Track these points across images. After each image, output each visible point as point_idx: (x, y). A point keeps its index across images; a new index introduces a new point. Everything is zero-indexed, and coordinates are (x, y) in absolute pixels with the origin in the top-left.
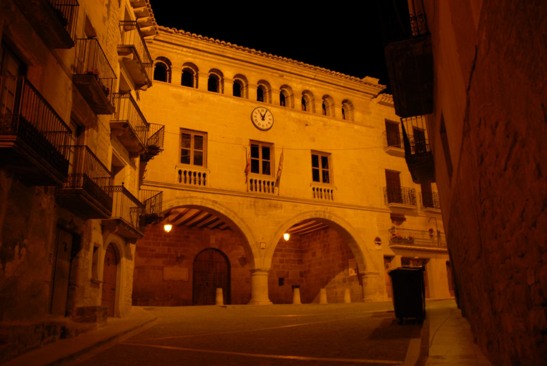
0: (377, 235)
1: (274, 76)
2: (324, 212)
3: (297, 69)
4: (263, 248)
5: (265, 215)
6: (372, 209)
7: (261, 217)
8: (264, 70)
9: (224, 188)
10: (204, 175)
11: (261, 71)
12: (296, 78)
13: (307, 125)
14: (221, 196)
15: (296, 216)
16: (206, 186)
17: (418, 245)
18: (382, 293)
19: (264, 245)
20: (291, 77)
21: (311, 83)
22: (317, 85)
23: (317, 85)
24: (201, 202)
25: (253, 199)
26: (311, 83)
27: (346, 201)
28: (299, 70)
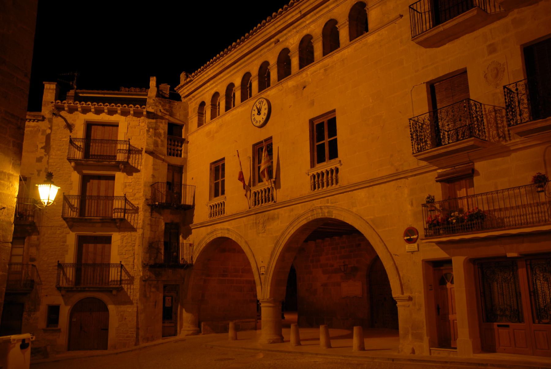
0: (410, 222)
1: (270, 49)
2: (321, 208)
3: (279, 23)
4: (263, 274)
6: (396, 176)
7: (261, 235)
8: (245, 62)
9: (234, 212)
10: (337, 170)
11: (260, 54)
12: (289, 31)
13: (304, 87)
15: (291, 225)
17: (515, 227)
19: (264, 270)
20: (285, 34)
24: (221, 233)
26: (307, 22)
28: (282, 22)
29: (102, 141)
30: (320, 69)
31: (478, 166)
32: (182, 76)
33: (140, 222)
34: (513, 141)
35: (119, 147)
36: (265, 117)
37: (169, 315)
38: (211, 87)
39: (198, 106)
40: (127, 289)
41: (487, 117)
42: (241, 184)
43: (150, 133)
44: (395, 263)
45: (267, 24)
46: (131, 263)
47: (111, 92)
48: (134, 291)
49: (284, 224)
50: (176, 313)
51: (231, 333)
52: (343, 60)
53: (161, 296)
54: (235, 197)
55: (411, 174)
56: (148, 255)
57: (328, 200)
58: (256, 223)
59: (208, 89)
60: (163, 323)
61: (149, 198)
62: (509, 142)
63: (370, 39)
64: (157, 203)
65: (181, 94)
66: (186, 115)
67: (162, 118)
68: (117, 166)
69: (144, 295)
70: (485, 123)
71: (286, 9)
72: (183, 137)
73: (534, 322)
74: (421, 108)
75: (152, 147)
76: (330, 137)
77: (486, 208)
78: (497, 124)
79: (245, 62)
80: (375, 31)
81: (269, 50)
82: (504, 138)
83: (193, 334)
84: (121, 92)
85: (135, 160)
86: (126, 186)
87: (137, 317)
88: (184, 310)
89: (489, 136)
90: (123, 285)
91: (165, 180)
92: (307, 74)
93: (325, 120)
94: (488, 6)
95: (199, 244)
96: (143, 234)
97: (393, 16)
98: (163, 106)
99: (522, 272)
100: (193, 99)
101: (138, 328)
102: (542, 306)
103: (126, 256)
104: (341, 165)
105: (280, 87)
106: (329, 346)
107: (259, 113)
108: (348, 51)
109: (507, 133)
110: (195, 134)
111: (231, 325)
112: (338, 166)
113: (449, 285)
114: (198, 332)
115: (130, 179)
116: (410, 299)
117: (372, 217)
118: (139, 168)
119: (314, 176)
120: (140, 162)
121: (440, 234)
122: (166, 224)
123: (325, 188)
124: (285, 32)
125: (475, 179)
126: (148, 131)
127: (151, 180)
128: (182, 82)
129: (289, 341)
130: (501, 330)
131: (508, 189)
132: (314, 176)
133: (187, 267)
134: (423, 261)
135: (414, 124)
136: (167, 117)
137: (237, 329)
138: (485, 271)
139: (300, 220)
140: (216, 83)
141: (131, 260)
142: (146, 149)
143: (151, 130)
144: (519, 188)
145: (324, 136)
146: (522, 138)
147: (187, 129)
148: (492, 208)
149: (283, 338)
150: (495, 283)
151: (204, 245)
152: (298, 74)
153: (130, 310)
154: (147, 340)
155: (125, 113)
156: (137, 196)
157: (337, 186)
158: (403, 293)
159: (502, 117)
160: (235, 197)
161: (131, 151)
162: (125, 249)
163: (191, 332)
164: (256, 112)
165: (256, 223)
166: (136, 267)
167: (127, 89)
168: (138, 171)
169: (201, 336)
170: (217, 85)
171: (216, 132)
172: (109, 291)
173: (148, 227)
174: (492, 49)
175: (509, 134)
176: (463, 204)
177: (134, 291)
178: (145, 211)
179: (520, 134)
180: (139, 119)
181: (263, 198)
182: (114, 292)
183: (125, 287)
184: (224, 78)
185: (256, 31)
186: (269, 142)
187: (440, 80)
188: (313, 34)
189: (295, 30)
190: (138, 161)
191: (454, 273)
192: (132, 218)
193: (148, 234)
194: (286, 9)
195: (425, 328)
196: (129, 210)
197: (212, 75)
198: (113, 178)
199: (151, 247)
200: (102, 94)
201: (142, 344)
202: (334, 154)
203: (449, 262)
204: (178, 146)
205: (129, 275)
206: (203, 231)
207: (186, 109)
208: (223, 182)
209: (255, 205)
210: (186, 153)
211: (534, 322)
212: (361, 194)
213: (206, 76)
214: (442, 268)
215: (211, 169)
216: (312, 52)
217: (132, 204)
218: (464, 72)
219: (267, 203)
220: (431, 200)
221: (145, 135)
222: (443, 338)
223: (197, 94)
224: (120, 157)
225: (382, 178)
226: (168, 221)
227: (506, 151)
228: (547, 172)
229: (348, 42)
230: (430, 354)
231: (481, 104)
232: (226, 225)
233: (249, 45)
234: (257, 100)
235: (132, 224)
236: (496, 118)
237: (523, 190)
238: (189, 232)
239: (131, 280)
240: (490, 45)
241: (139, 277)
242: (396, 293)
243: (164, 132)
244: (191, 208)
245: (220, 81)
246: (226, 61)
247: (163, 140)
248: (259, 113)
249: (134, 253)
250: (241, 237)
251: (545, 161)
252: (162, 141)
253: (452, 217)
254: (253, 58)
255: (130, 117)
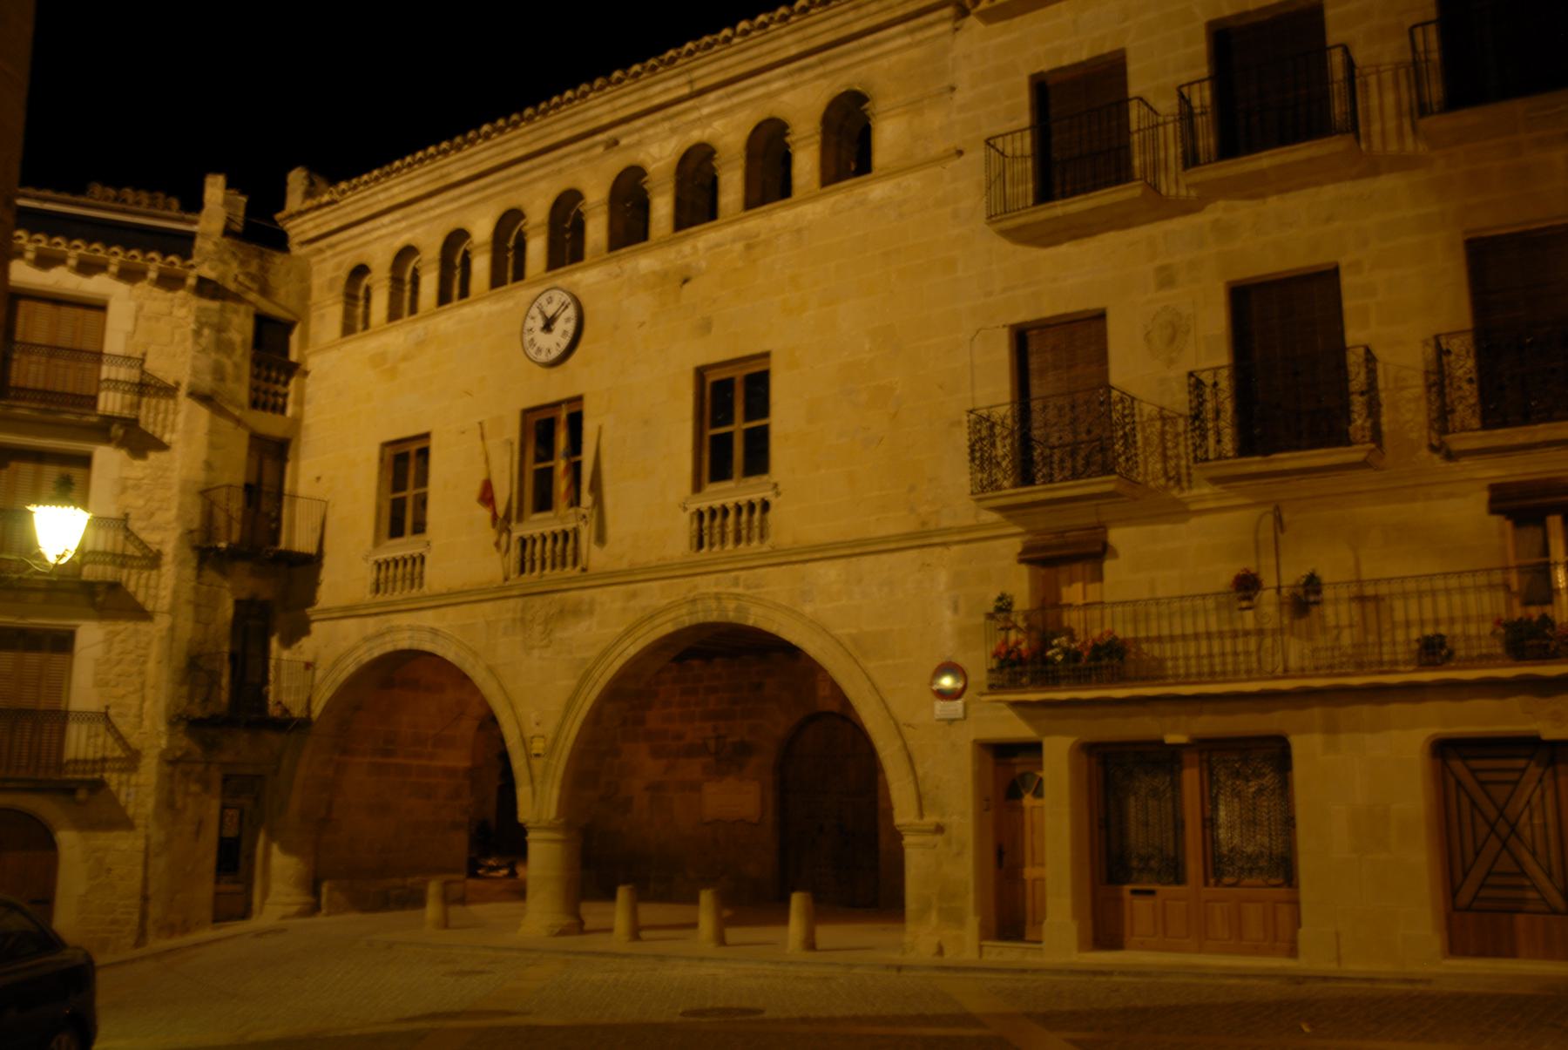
0: (949, 649)
3: (626, 100)
4: (538, 755)
5: (547, 646)
6: (922, 539)
7: (536, 653)
8: (508, 178)
10: (766, 506)
11: (555, 167)
13: (686, 281)
14: (450, 610)
15: (628, 633)
16: (425, 588)
18: (953, 917)
21: (705, 111)
22: (726, 104)
23: (726, 104)
24: (691, 613)
25: (520, 601)
26: (705, 111)
27: (816, 533)
28: (635, 97)
29: (53, 350)
30: (734, 241)
31: (1116, 536)
32: (297, 179)
33: (165, 596)
34: (1195, 492)
35: (107, 371)
36: (565, 342)
37: (233, 860)
38: (391, 229)
39: (343, 274)
40: (120, 784)
41: (1143, 430)
42: (484, 514)
43: (203, 341)
44: (905, 746)
45: (591, 95)
46: (134, 711)
47: (67, 197)
48: (139, 791)
49: (609, 628)
50: (251, 857)
51: (432, 910)
52: (799, 231)
53: (215, 805)
54: (458, 539)
55: (957, 538)
56: (184, 690)
57: (737, 578)
58: (522, 620)
59: (384, 231)
60: (217, 882)
61: (195, 525)
62: (1186, 494)
63: (875, 190)
64: (223, 545)
65: (291, 233)
66: (305, 295)
67: (237, 298)
68: (104, 430)
69: (168, 805)
70: (1140, 444)
71: (654, 68)
72: (293, 357)
73: (1206, 884)
74: (997, 393)
75: (207, 383)
76: (749, 416)
77: (1130, 634)
78: (1165, 448)
79: (508, 178)
80: (889, 174)
81: (587, 161)
82: (1179, 481)
83: (302, 914)
84: (91, 201)
85: (157, 414)
86: (124, 490)
87: (146, 865)
88: (275, 848)
89: (1146, 474)
90: (106, 775)
91: (239, 478)
92: (695, 248)
93: (739, 374)
94: (1163, 178)
95: (335, 664)
96: (172, 628)
97: (938, 148)
98: (242, 263)
99: (1191, 778)
100: (329, 253)
101: (145, 899)
102: (1225, 850)
103: (121, 691)
104: (778, 494)
105: (613, 267)
106: (721, 940)
107: (548, 326)
108: (813, 209)
109: (1184, 471)
110: (334, 355)
111: (433, 888)
112: (769, 495)
113: (1028, 800)
114: (315, 909)
115: (138, 469)
116: (939, 829)
117: (854, 631)
118: (167, 438)
119: (700, 515)
120: (169, 423)
121: (1022, 686)
122: (238, 603)
123: (730, 546)
124: (639, 123)
125: (1109, 565)
126: (197, 333)
127: (200, 476)
128: (294, 201)
129: (610, 930)
130: (1141, 904)
131: (1182, 597)
132: (700, 515)
133: (286, 724)
134: (975, 741)
135: (982, 430)
136: (253, 296)
137: (447, 900)
138: (1113, 769)
139: (658, 622)
140: (412, 221)
141: (133, 700)
142: (190, 385)
143: (206, 332)
144: (1204, 596)
145: (732, 415)
146: (1217, 489)
147: (305, 338)
148: (1142, 634)
149: (582, 923)
150: (1132, 800)
151: (351, 669)
152: (669, 242)
153: (125, 845)
154: (171, 929)
155: (129, 275)
156: (159, 518)
157: (765, 548)
158: (921, 815)
159: (1177, 435)
160: (458, 539)
161: (147, 387)
162: (117, 669)
163: (295, 909)
164: (540, 323)
165: (522, 620)
166: (147, 723)
167: (112, 192)
168: (162, 446)
169: (320, 919)
170: (413, 226)
171: (405, 358)
172: (67, 790)
173: (187, 612)
174: (1166, 278)
175: (1189, 475)
176: (1072, 619)
177: (139, 791)
178: (181, 563)
179: (1215, 481)
180: (170, 295)
181: (548, 554)
182: (82, 795)
183: (113, 779)
184: (438, 211)
185: (557, 106)
186: (574, 409)
187: (1044, 325)
188: (719, 145)
189: (667, 125)
190: (165, 419)
191: (1046, 774)
192: (143, 581)
193: (187, 629)
194: (654, 68)
195: (971, 897)
196: (133, 557)
197: (402, 199)
198: (85, 461)
199: (194, 668)
200: (37, 198)
201: (157, 943)
202: (758, 461)
203: (1034, 748)
204: (277, 382)
205: (125, 745)
206: (351, 629)
207: (305, 277)
208: (422, 502)
209: (522, 571)
210: (300, 402)
211: (1206, 884)
212: (829, 573)
213: (381, 196)
214: (1015, 760)
215: (382, 460)
216: (711, 188)
217: (142, 542)
218: (1101, 316)
219: (557, 571)
220: (1004, 606)
221: (189, 343)
222: (1010, 918)
223: (345, 241)
224: (110, 403)
225: (885, 539)
226: (244, 595)
227: (1179, 512)
228: (1258, 567)
229: (816, 185)
230: (981, 955)
231: (1133, 399)
232: (428, 619)
233: (529, 138)
234: (544, 293)
235: (140, 598)
236: (1163, 433)
237: (1211, 603)
238: (302, 629)
239: (132, 759)
240: (1162, 269)
241: (156, 751)
242: (903, 811)
243: (244, 342)
244: (311, 563)
245: (424, 216)
246: (452, 168)
247: (239, 363)
248: (548, 326)
249: (143, 685)
250: (476, 654)
251: (1257, 542)
252: (236, 365)
253: (1053, 647)
254: (535, 174)
255: (143, 288)
